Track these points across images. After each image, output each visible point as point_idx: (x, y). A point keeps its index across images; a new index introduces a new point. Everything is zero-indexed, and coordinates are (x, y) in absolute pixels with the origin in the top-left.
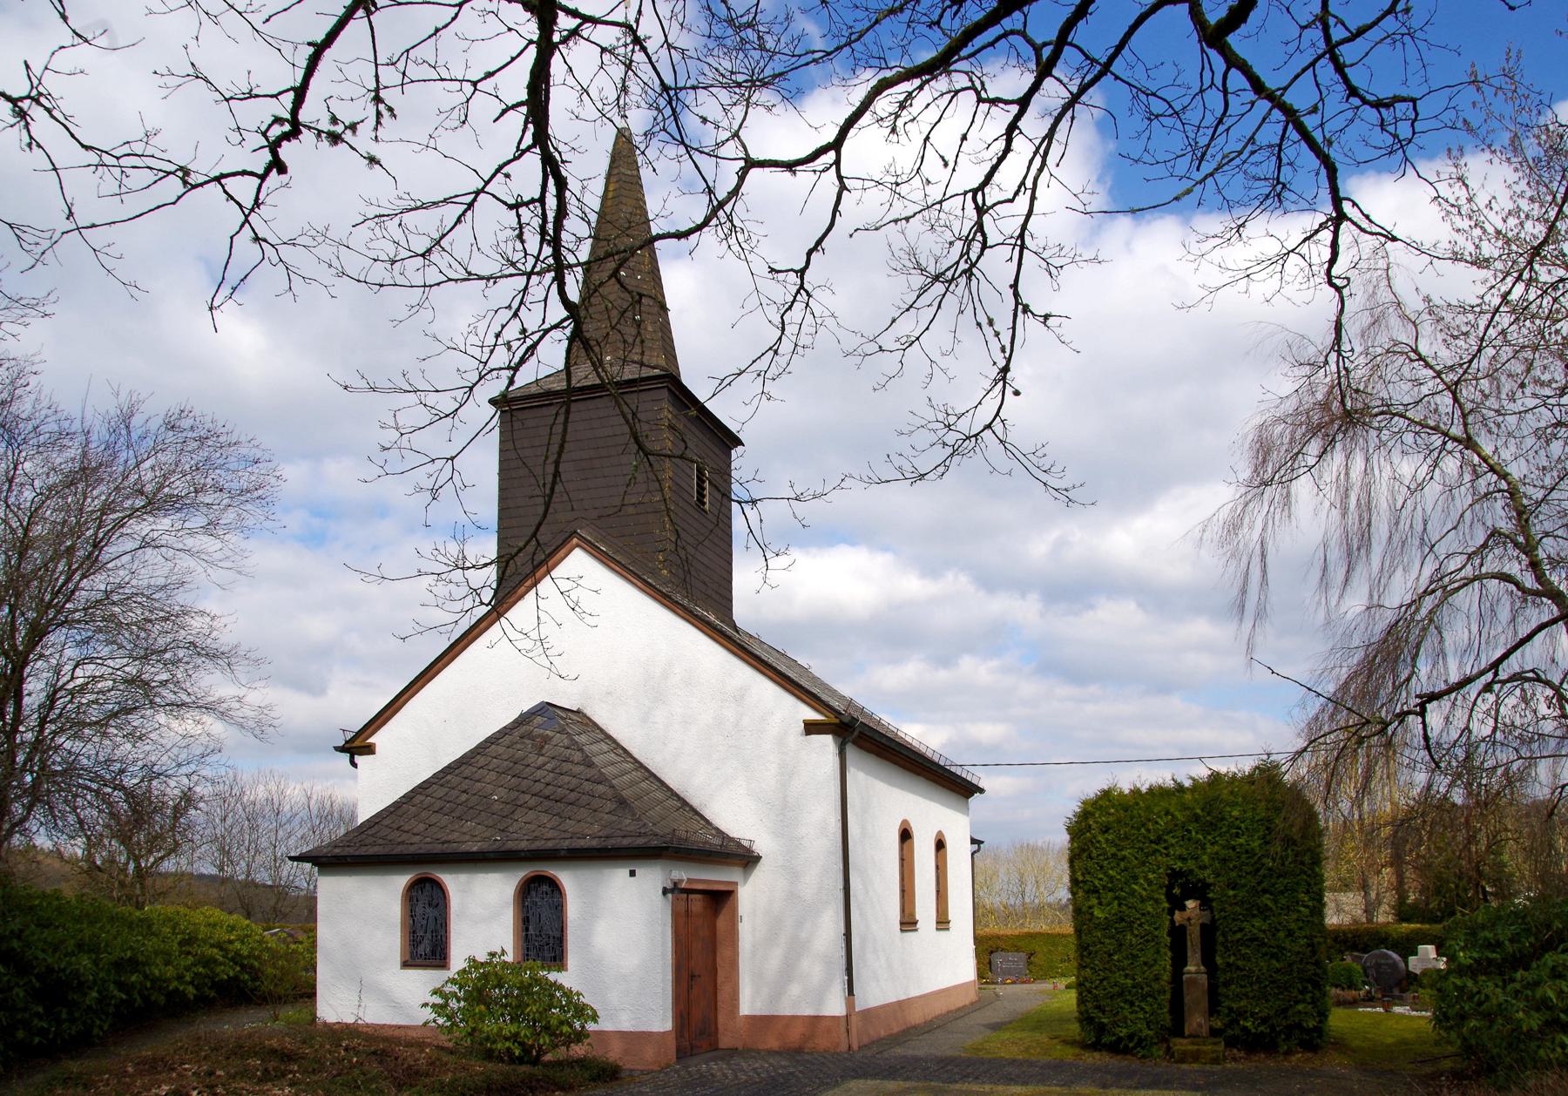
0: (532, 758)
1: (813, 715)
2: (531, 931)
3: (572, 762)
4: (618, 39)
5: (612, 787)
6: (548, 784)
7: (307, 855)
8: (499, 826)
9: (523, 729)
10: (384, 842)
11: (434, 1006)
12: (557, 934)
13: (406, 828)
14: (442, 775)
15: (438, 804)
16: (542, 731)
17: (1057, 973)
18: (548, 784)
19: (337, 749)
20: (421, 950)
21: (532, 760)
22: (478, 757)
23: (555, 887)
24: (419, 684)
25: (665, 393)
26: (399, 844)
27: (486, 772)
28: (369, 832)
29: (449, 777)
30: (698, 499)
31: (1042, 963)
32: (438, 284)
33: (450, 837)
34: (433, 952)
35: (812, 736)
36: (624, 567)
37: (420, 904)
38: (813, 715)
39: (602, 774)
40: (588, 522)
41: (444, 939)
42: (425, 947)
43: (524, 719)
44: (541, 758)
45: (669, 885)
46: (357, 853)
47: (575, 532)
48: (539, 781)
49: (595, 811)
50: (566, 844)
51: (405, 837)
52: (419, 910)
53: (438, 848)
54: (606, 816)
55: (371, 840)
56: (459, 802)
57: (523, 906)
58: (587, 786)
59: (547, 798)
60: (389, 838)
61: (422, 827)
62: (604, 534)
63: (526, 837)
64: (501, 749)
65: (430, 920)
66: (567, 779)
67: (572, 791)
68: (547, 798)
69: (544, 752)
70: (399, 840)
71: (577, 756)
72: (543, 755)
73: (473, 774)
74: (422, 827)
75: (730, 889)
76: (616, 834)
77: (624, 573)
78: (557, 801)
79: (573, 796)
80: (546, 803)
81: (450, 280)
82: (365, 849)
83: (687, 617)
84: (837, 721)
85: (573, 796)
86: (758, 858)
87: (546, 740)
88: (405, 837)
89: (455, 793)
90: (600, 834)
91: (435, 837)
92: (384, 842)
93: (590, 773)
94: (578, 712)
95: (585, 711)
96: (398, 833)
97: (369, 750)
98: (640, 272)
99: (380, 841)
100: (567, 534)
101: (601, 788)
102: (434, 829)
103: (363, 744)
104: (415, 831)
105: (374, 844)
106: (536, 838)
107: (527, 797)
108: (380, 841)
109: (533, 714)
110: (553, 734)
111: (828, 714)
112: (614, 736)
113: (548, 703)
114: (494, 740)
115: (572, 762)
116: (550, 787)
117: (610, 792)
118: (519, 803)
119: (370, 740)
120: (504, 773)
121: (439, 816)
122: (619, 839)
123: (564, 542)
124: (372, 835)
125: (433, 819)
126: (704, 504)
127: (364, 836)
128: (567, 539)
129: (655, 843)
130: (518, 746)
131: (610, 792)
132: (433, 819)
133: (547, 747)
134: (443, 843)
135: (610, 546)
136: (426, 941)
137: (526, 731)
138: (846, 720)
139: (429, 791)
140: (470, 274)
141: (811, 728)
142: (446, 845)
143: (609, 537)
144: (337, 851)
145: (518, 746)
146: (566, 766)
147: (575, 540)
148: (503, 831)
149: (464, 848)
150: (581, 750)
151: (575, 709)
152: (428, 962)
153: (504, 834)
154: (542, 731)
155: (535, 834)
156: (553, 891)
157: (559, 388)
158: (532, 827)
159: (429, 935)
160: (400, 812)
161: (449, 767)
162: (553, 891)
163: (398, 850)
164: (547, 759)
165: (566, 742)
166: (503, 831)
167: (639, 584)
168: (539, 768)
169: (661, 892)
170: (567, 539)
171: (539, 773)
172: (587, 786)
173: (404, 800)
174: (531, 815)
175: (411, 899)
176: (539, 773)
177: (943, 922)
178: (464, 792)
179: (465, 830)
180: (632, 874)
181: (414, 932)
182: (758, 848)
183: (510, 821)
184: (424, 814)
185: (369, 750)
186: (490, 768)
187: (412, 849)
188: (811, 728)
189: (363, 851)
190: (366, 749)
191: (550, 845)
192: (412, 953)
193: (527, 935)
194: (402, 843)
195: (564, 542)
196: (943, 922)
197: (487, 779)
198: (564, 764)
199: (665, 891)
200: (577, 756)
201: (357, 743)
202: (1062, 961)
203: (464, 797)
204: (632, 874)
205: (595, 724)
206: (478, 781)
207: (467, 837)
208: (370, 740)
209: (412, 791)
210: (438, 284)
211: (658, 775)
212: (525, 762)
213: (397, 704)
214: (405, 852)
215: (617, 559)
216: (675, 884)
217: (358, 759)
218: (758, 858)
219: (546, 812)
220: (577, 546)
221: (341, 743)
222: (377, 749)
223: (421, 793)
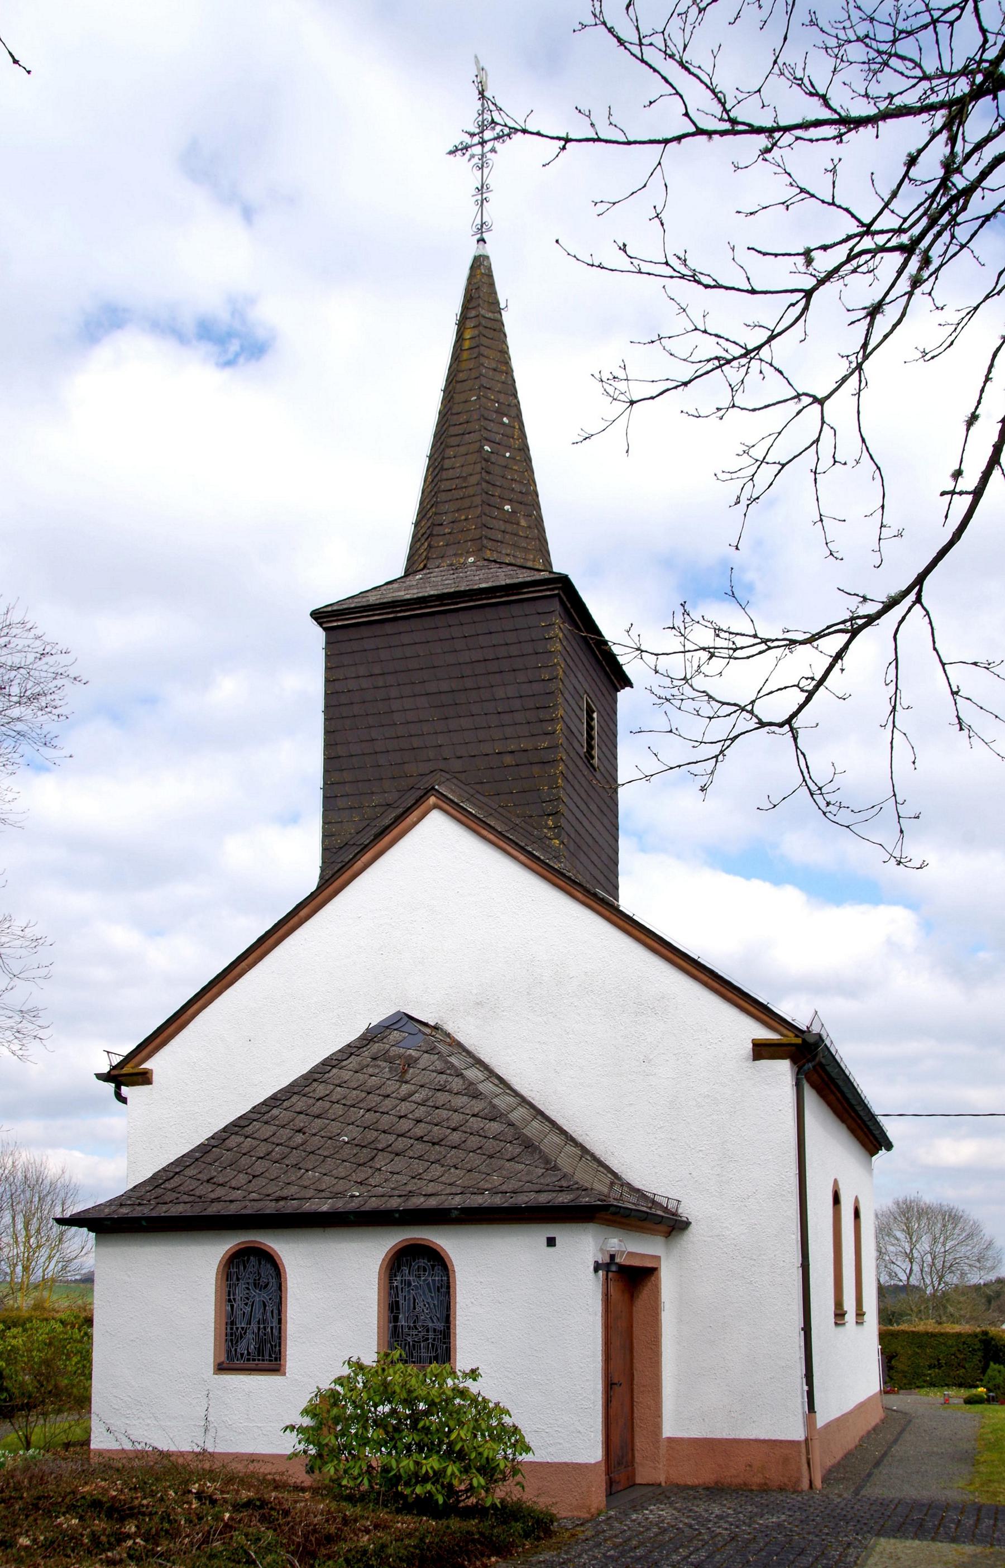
0: (391, 1086)
1: (765, 1034)
2: (402, 1322)
3: (450, 1091)
4: (493, 150)
5: (511, 1124)
6: (419, 1121)
7: (82, 1216)
8: (354, 1176)
9: (375, 1047)
10: (191, 1199)
11: (301, 1430)
12: (440, 1326)
13: (221, 1180)
14: (265, 1109)
15: (263, 1149)
16: (402, 1050)
17: (925, 1381)
18: (419, 1121)
19: (100, 1076)
20: (242, 1348)
21: (393, 1088)
22: (315, 1084)
23: (272, 1263)
24: (215, 990)
25: (556, 605)
26: (212, 1201)
27: (328, 1105)
28: (167, 1185)
29: (275, 1112)
30: (588, 751)
31: (906, 1369)
32: (679, 139)
33: (285, 1193)
34: (260, 1351)
35: (762, 1061)
36: (500, 834)
37: (242, 1284)
38: (765, 1034)
39: (494, 1106)
40: (448, 776)
41: (276, 1332)
42: (248, 1344)
43: (371, 1037)
44: (405, 1086)
45: (605, 1259)
46: (154, 1214)
47: (433, 788)
48: (405, 1116)
49: (491, 1157)
50: (457, 1201)
51: (220, 1192)
52: (240, 1292)
53: (270, 1208)
54: (508, 1164)
55: (170, 1196)
56: (294, 1145)
57: (391, 1288)
58: (475, 1123)
59: (420, 1139)
60: (197, 1193)
61: (242, 1178)
62: (472, 791)
63: (397, 1192)
64: (346, 1075)
65: (256, 1305)
66: (444, 1114)
67: (454, 1130)
68: (420, 1139)
69: (408, 1077)
70: (213, 1196)
71: (456, 1084)
72: (406, 1082)
73: (309, 1107)
74: (242, 1178)
75: (649, 1264)
76: (525, 1189)
77: (501, 843)
78: (434, 1144)
79: (456, 1137)
80: (419, 1146)
81: (700, 132)
82: (164, 1208)
83: (588, 901)
84: (799, 1041)
85: (456, 1137)
86: (687, 1224)
87: (410, 1062)
88: (220, 1192)
89: (286, 1133)
90: (504, 1188)
91: (265, 1191)
92: (191, 1199)
93: (477, 1106)
94: (436, 1028)
95: (445, 1027)
96: (209, 1187)
97: (144, 1078)
98: (509, 448)
99: (185, 1198)
100: (420, 793)
101: (495, 1127)
102: (261, 1181)
103: (136, 1071)
104: (234, 1183)
105: (177, 1202)
106: (411, 1194)
107: (391, 1138)
108: (185, 1198)
109: (387, 1027)
110: (419, 1054)
111: (786, 1032)
112: (486, 1060)
113: (405, 1014)
114: (334, 1063)
115: (450, 1091)
116: (422, 1125)
117: (510, 1132)
118: (380, 1146)
119: (146, 1065)
120: (353, 1106)
121: (266, 1163)
122: (533, 1195)
123: (417, 801)
124: (173, 1190)
125: (260, 1167)
126: (593, 758)
127: (160, 1191)
128: (421, 797)
129: (585, 1200)
130: (371, 1070)
131: (510, 1132)
132: (260, 1167)
133: (411, 1070)
134: (277, 1200)
135: (480, 808)
136: (250, 1336)
137: (379, 1051)
138: (811, 1040)
139: (249, 1130)
140: (733, 122)
141: (761, 1051)
142: (282, 1203)
143: (478, 796)
144: (124, 1211)
145: (371, 1070)
146: (442, 1098)
147: (432, 800)
148: (361, 1183)
149: (308, 1207)
150: (460, 1075)
151: (432, 1024)
152: (252, 1364)
153: (363, 1189)
154: (402, 1050)
155: (409, 1188)
156: (433, 1266)
157: (408, 597)
158: (404, 1179)
159: (254, 1326)
160: (209, 1158)
161: (274, 1098)
162: (433, 1266)
163: (213, 1209)
164: (413, 1088)
165: (439, 1065)
166: (361, 1183)
167: (522, 858)
168: (403, 1100)
169: (592, 1268)
170: (421, 797)
171: (404, 1107)
172: (475, 1123)
173: (213, 1142)
174: (399, 1164)
175: (228, 1276)
176: (404, 1107)
177: (860, 1314)
178: (299, 1131)
179: (305, 1184)
180: (551, 1242)
181: (232, 1323)
182: (686, 1211)
183: (370, 1171)
184: (245, 1161)
185: (144, 1078)
186: (334, 1098)
187: (233, 1209)
188: (761, 1051)
189: (162, 1211)
190: (140, 1079)
191: (432, 1203)
192: (229, 1352)
193: (395, 1327)
194: (218, 1200)
195: (417, 801)
196: (860, 1314)
197: (331, 1114)
198: (439, 1094)
199: (597, 1267)
200: (456, 1084)
201: (127, 1070)
202: (930, 1367)
203: (299, 1138)
204: (551, 1242)
205: (459, 1045)
206: (318, 1117)
207: (310, 1193)
208: (146, 1065)
209: (225, 1130)
210: (679, 139)
211: (547, 1113)
212: (381, 1092)
213: (184, 1018)
214: (223, 1213)
215: (492, 824)
216: (612, 1257)
217: (125, 1090)
218: (687, 1224)
219: (419, 1158)
220: (435, 806)
221: (105, 1069)
222: (155, 1078)
223: (236, 1134)
